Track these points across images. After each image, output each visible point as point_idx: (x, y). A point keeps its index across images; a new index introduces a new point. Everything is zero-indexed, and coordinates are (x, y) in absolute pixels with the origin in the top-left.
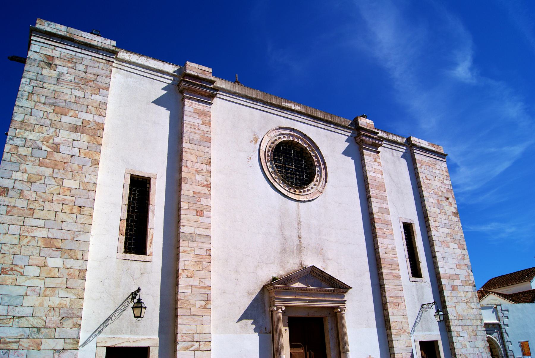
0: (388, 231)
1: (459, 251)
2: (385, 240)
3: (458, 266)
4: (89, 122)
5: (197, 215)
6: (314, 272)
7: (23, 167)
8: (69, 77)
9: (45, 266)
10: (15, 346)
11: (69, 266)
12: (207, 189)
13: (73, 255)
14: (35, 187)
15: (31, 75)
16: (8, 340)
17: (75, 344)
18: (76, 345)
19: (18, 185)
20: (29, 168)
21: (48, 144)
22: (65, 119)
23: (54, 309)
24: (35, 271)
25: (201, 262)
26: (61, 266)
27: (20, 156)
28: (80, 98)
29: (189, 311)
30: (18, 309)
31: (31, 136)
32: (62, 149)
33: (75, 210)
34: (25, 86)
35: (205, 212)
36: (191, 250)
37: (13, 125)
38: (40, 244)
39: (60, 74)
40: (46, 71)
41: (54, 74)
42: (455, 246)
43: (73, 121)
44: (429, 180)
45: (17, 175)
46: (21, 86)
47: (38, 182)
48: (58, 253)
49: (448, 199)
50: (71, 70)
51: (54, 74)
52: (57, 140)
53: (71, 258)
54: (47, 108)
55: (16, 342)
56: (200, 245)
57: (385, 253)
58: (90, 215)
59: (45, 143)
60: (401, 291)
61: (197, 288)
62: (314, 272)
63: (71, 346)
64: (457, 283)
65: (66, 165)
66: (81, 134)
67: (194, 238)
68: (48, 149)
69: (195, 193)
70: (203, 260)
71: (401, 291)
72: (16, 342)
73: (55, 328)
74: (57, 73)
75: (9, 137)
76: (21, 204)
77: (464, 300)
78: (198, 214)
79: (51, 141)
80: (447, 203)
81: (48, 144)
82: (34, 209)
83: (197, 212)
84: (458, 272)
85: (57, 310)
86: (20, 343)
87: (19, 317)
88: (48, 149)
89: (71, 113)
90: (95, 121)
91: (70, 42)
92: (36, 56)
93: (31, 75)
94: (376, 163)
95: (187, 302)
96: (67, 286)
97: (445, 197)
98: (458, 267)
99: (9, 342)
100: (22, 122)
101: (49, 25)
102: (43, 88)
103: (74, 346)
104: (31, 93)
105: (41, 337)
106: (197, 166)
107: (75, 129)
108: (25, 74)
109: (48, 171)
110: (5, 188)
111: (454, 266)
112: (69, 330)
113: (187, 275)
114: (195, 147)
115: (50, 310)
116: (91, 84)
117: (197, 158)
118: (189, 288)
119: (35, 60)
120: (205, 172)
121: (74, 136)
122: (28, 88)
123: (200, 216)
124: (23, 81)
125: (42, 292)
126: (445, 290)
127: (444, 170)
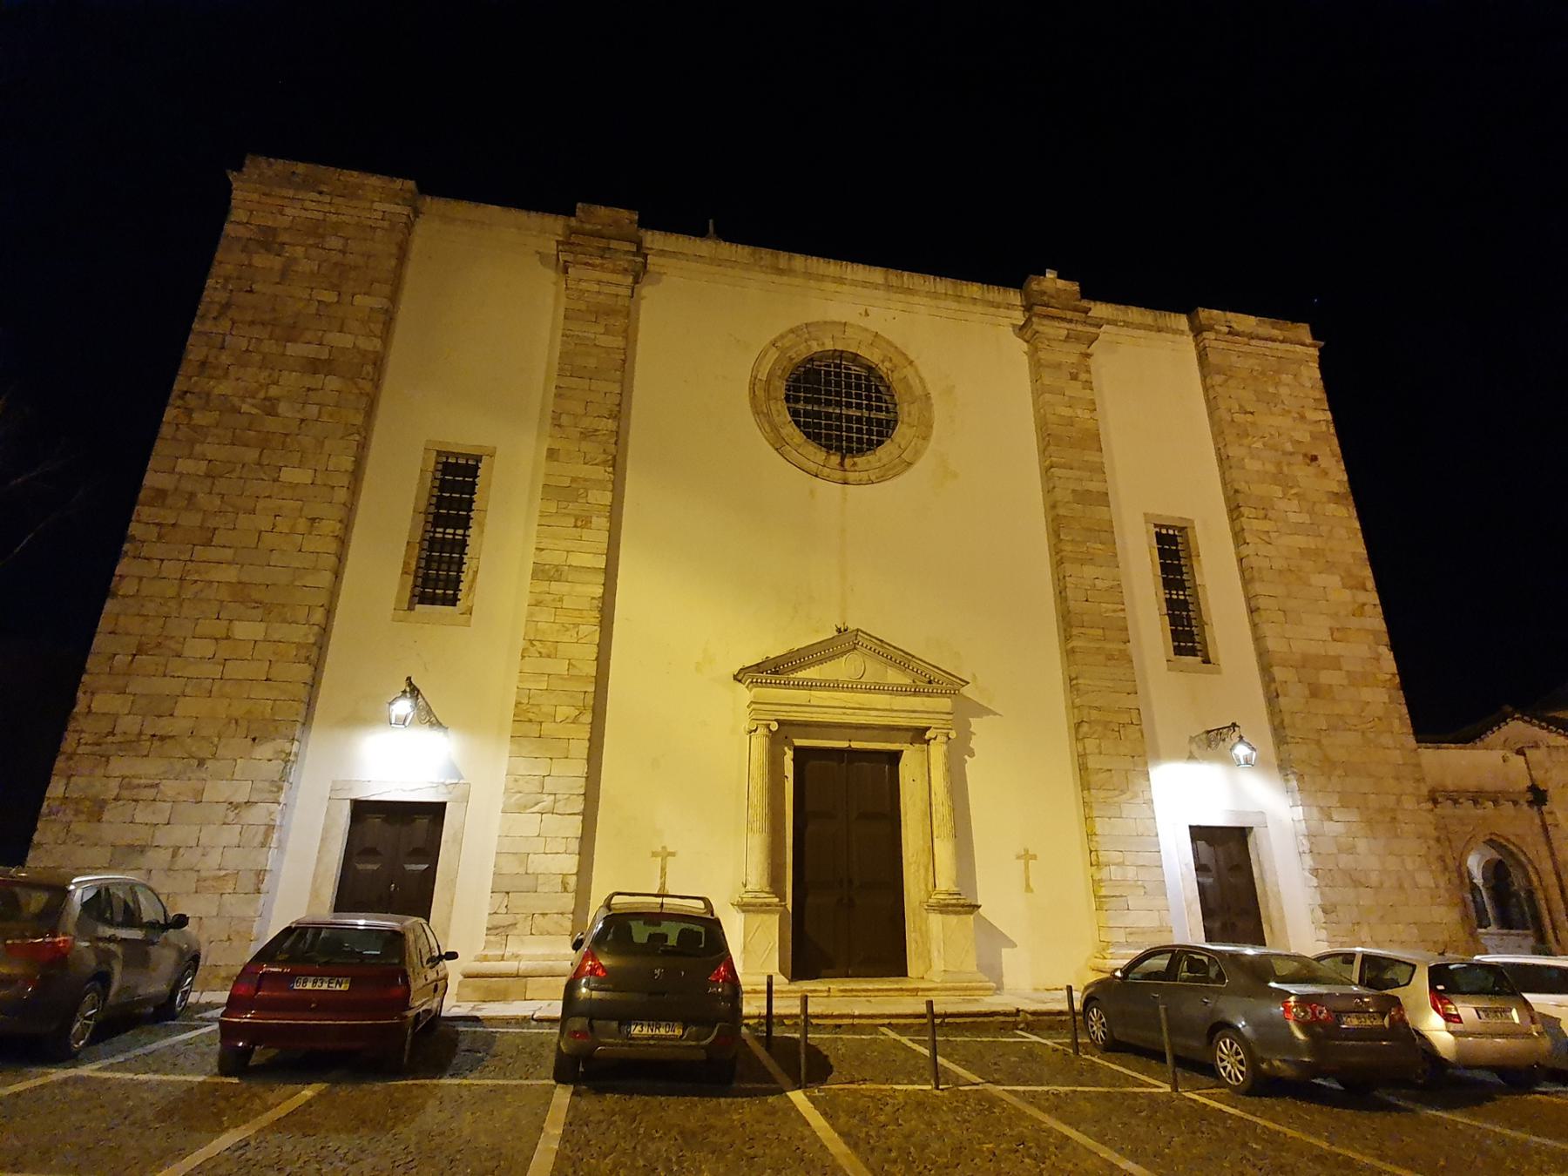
0: (1100, 546)
1: (1347, 595)
2: (1085, 568)
3: (1339, 634)
4: (344, 350)
5: (575, 526)
6: (891, 658)
7: (198, 448)
8: (306, 266)
9: (228, 638)
10: (151, 793)
11: (276, 637)
12: (605, 471)
13: (289, 614)
14: (221, 485)
15: (229, 268)
16: (136, 781)
17: (275, 792)
18: (276, 795)
19: (187, 486)
20: (210, 450)
21: (254, 401)
22: (293, 349)
23: (236, 722)
24: (207, 648)
25: (576, 625)
26: (260, 637)
27: (194, 428)
28: (328, 305)
29: (536, 727)
30: (164, 721)
31: (223, 388)
32: (283, 408)
33: (302, 525)
34: (214, 294)
35: (594, 519)
36: (554, 600)
37: (185, 369)
38: (224, 594)
39: (293, 260)
40: (260, 260)
41: (277, 263)
42: (1334, 581)
43: (310, 351)
44: (1252, 413)
45: (184, 465)
46: (205, 293)
47: (227, 475)
48: (259, 613)
49: (1314, 458)
50: (313, 252)
51: (277, 263)
52: (274, 391)
53: (284, 621)
54: (256, 332)
55: (152, 786)
56: (579, 588)
57: (1087, 601)
58: (331, 534)
59: (249, 400)
60: (1129, 694)
61: (562, 679)
62: (891, 658)
63: (267, 796)
64: (1327, 677)
65: (288, 440)
66: (326, 376)
67: (564, 574)
68: (254, 411)
69: (574, 480)
70: (579, 621)
71: (1129, 694)
72: (152, 786)
73: (236, 760)
74: (283, 259)
75: (174, 394)
76: (191, 520)
77: (1355, 726)
78: (579, 523)
79: (262, 395)
80: (1311, 470)
81: (254, 401)
82: (215, 529)
83: (576, 520)
84: (1335, 649)
85: (243, 723)
86: (161, 786)
87: (163, 738)
88: (254, 411)
89: (308, 336)
90: (358, 348)
91: (826, 979)
92: (242, 232)
93: (229, 268)
94: (1078, 385)
95: (535, 709)
96: (269, 677)
97: (1305, 455)
98: (1336, 635)
99: (139, 786)
100: (203, 364)
101: (270, 165)
102: (251, 291)
103: (271, 797)
104: (227, 306)
105: (204, 775)
106: (586, 423)
107: (314, 366)
108: (215, 270)
109: (251, 455)
110: (158, 490)
111: (1326, 635)
112: (265, 765)
113: (540, 653)
114: (585, 383)
115: (229, 723)
116: (353, 274)
117: (586, 406)
118: (543, 679)
119: (238, 239)
120: (604, 435)
121: (309, 381)
122: (221, 297)
123: (582, 527)
124: (210, 282)
125: (215, 688)
126: (1285, 696)
127: (1309, 385)
